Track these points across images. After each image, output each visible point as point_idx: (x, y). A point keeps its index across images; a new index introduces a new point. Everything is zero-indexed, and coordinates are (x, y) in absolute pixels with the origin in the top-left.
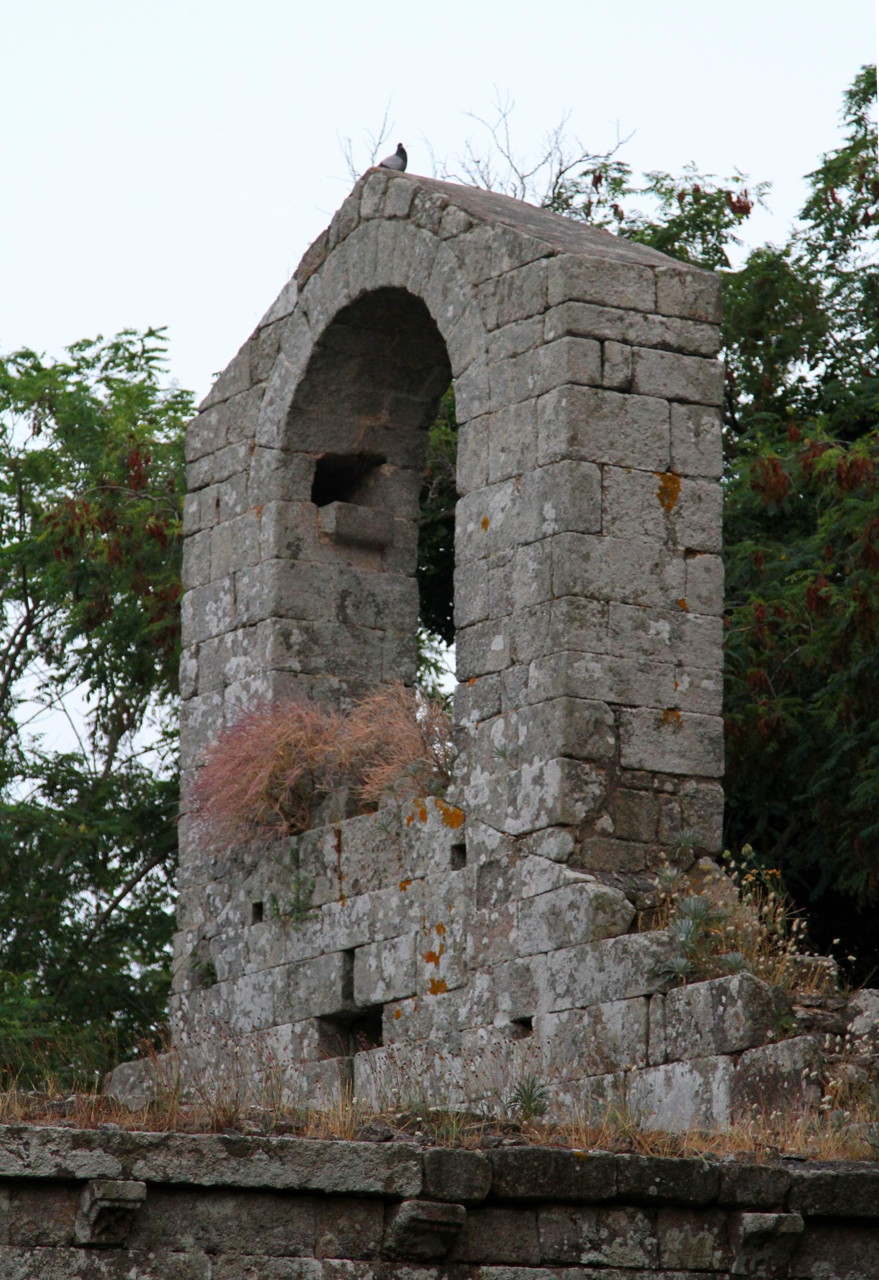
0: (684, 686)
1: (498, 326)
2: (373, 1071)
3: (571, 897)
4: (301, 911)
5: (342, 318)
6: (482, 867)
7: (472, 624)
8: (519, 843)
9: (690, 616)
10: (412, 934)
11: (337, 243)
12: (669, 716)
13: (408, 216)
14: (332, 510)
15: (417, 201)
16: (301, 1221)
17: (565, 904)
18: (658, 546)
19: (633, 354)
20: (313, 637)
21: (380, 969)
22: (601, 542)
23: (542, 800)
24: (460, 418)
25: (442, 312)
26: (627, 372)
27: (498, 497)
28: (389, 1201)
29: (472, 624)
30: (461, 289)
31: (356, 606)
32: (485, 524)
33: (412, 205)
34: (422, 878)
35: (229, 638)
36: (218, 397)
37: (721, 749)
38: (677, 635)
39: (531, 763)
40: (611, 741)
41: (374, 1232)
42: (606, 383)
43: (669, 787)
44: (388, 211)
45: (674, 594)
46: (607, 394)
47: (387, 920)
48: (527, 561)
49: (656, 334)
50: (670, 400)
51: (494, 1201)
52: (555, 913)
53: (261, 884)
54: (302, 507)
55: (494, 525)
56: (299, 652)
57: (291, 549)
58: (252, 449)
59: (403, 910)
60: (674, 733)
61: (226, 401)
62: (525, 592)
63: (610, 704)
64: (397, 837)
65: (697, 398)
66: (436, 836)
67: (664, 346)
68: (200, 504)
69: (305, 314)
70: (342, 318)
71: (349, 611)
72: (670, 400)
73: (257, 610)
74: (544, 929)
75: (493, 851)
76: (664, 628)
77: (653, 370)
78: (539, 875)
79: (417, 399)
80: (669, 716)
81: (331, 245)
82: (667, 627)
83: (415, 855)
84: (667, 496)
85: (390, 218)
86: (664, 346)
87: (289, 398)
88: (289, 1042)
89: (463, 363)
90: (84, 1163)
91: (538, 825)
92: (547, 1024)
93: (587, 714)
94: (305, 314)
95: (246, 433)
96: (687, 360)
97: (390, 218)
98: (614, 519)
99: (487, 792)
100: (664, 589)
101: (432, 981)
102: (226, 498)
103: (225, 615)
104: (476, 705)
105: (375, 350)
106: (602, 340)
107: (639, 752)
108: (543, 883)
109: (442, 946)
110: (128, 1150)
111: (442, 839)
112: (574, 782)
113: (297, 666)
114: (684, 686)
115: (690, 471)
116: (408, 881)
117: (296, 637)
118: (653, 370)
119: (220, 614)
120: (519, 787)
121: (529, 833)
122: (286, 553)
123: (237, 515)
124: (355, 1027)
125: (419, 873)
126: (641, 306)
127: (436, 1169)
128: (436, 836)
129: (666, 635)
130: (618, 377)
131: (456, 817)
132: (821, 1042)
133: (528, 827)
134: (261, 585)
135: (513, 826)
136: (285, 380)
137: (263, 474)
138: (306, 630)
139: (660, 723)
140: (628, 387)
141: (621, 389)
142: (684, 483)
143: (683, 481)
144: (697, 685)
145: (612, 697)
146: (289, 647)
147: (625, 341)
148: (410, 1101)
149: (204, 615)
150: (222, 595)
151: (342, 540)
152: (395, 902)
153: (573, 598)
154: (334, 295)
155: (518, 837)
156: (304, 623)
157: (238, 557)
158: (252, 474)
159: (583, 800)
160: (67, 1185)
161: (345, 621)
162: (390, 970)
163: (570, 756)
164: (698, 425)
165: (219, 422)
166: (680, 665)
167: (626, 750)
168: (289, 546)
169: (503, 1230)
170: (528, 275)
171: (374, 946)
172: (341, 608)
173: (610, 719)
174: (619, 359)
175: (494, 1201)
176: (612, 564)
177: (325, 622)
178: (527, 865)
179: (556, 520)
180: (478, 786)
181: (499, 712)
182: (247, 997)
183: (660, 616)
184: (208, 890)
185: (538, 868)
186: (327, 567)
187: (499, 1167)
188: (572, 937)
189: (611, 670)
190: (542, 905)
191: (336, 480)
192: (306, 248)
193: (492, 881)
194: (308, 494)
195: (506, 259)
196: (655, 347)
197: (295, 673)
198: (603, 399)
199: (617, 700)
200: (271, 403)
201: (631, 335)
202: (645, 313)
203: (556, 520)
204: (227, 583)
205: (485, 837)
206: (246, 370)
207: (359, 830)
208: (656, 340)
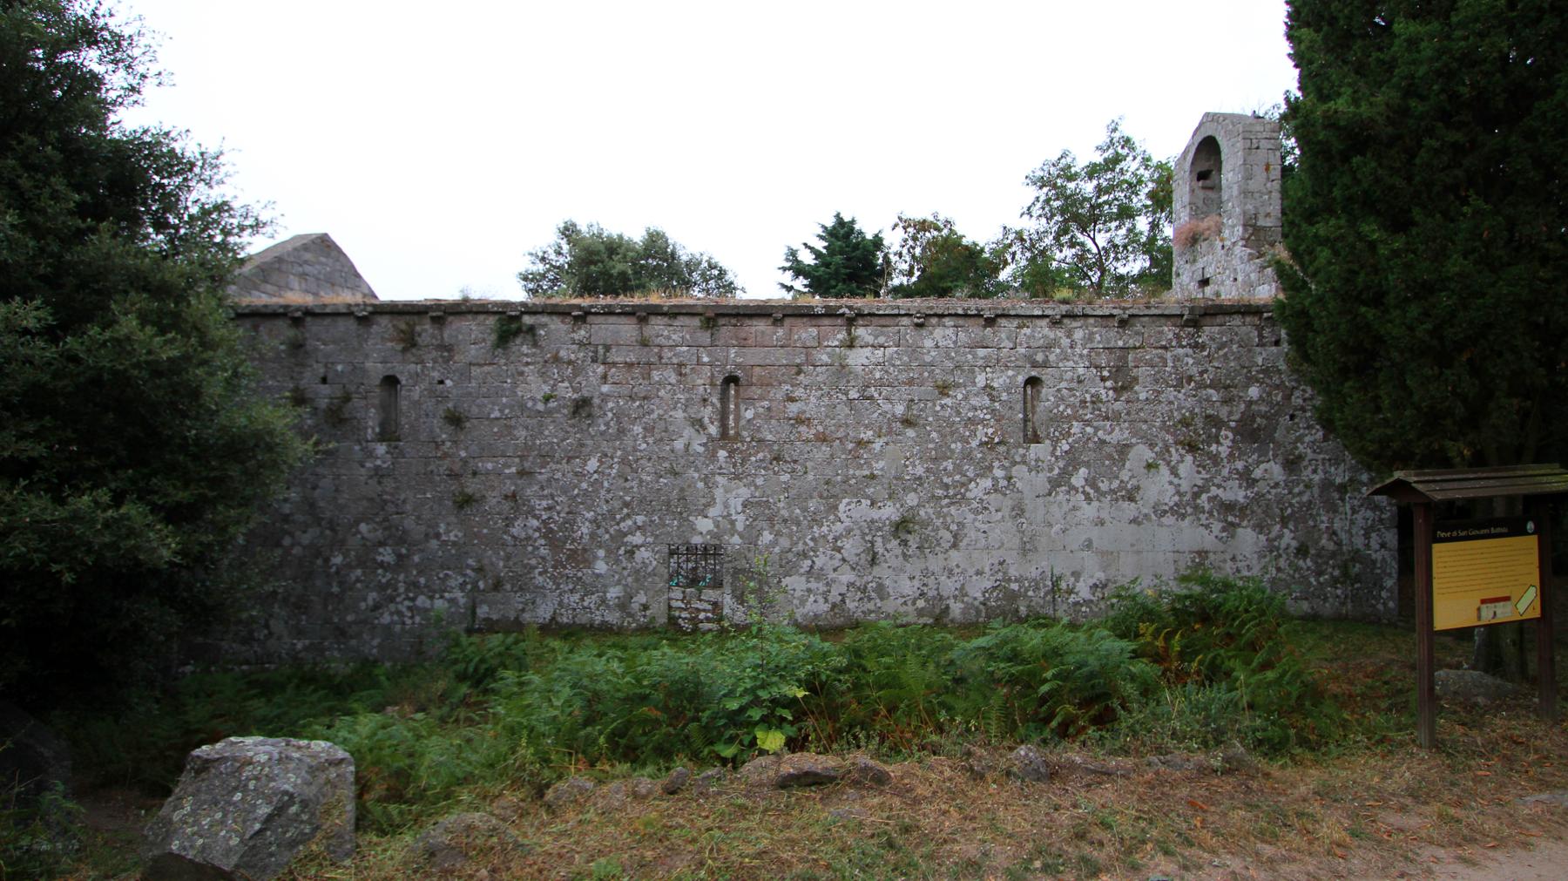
2: (1208, 290)
4: (1195, 261)
5: (1200, 144)
8: (1234, 244)
12: (1268, 215)
16: (1163, 320)
25: (1219, 139)
28: (1182, 316)
41: (1179, 321)
47: (1210, 261)
48: (1235, 187)
51: (1205, 314)
53: (1187, 257)
54: (1195, 182)
57: (1192, 191)
62: (1235, 192)
64: (1211, 246)
66: (1218, 244)
77: (1264, 144)
78: (1238, 249)
80: (1268, 215)
84: (1267, 169)
88: (1193, 286)
90: (1115, 312)
92: (1240, 279)
105: (1207, 150)
107: (1261, 223)
110: (1124, 309)
112: (1245, 230)
118: (1264, 144)
120: (1234, 231)
124: (1205, 282)
127: (1192, 309)
128: (1218, 244)
134: (1186, 199)
144: (1274, 206)
148: (156, 335)
149: (1176, 205)
151: (1204, 188)
153: (1246, 193)
154: (1199, 139)
157: (1182, 192)
160: (1112, 316)
163: (1245, 226)
169: (1208, 320)
175: (1205, 314)
176: (1253, 185)
177: (1200, 204)
180: (1226, 233)
182: (1185, 278)
186: (1201, 194)
187: (1207, 308)
191: (1202, 176)
192: (1286, 47)
193: (1229, 251)
205: (1228, 243)
207: (1204, 244)
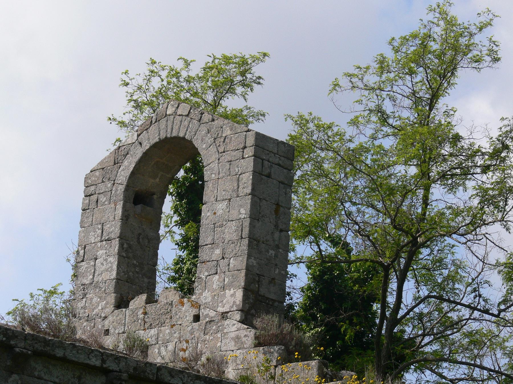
0: (277, 272)
1: (224, 152)
3: (246, 333)
6: (207, 322)
7: (207, 245)
9: (280, 250)
10: (175, 342)
11: (156, 122)
13: (187, 116)
14: (139, 207)
15: (191, 111)
17: (242, 335)
18: (273, 227)
19: (271, 166)
20: (130, 246)
21: (159, 353)
22: (258, 223)
23: (234, 302)
24: (206, 179)
26: (269, 171)
27: (220, 205)
29: (207, 245)
30: (209, 140)
31: (143, 239)
32: (215, 213)
33: (189, 112)
34: (180, 325)
35: (99, 244)
36: (100, 167)
37: (55, 328)
38: (276, 256)
39: (230, 290)
40: (257, 286)
42: (263, 173)
43: (271, 303)
44: (178, 113)
45: (276, 243)
46: (263, 177)
49: (277, 161)
50: (279, 182)
52: (238, 338)
55: (218, 214)
56: (126, 250)
58: (114, 184)
59: (171, 334)
60: (273, 286)
61: (103, 169)
63: (257, 274)
65: (286, 182)
67: (279, 165)
68: (89, 201)
69: (140, 144)
70: (155, 146)
71: (141, 240)
72: (279, 182)
73: (113, 236)
74: (233, 343)
75: (212, 317)
76: (272, 252)
79: (168, 176)
81: (154, 122)
82: (274, 252)
83: (178, 317)
85: (180, 115)
86: (279, 165)
87: (132, 169)
89: (209, 162)
91: (232, 310)
93: (251, 276)
94: (140, 144)
95: (111, 179)
96: (285, 171)
97: (180, 115)
98: (262, 216)
99: (210, 298)
100: (274, 240)
101: (182, 357)
102: (102, 199)
103: (98, 236)
104: (207, 270)
106: (263, 160)
107: (263, 291)
108: (234, 328)
109: (187, 347)
111: (190, 312)
113: (125, 255)
114: (277, 272)
115: (283, 205)
116: (174, 325)
117: (125, 246)
119: (96, 236)
121: (227, 312)
122: (124, 218)
123: (105, 205)
125: (179, 323)
126: (273, 151)
129: (273, 255)
130: (266, 172)
131: (197, 305)
132: (436, 368)
133: (228, 310)
135: (221, 309)
136: (130, 163)
137: (118, 192)
138: (128, 244)
139: (270, 282)
140: (269, 176)
141: (266, 176)
142: (281, 208)
143: (281, 208)
145: (258, 272)
146: (123, 249)
147: (269, 161)
150: (97, 230)
152: (168, 331)
154: (152, 137)
155: (223, 313)
156: (128, 242)
158: (113, 192)
159: (248, 303)
161: (139, 242)
162: (164, 353)
164: (286, 191)
165: (99, 175)
166: (276, 265)
167: (261, 289)
168: (126, 216)
170: (238, 137)
171: (157, 345)
172: (138, 238)
173: (257, 279)
174: (267, 166)
178: (227, 322)
179: (245, 214)
181: (216, 273)
183: (272, 249)
184: (85, 324)
185: (232, 324)
188: (245, 346)
189: (258, 263)
190: (233, 335)
194: (132, 200)
195: (229, 131)
196: (276, 164)
197: (124, 257)
198: (262, 179)
199: (259, 273)
200: (123, 170)
201: (271, 160)
202: (275, 154)
203: (245, 214)
204: (100, 226)
205: (207, 313)
206: (112, 159)
208: (277, 162)
